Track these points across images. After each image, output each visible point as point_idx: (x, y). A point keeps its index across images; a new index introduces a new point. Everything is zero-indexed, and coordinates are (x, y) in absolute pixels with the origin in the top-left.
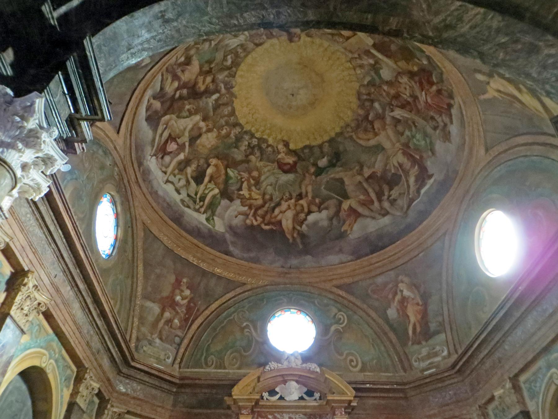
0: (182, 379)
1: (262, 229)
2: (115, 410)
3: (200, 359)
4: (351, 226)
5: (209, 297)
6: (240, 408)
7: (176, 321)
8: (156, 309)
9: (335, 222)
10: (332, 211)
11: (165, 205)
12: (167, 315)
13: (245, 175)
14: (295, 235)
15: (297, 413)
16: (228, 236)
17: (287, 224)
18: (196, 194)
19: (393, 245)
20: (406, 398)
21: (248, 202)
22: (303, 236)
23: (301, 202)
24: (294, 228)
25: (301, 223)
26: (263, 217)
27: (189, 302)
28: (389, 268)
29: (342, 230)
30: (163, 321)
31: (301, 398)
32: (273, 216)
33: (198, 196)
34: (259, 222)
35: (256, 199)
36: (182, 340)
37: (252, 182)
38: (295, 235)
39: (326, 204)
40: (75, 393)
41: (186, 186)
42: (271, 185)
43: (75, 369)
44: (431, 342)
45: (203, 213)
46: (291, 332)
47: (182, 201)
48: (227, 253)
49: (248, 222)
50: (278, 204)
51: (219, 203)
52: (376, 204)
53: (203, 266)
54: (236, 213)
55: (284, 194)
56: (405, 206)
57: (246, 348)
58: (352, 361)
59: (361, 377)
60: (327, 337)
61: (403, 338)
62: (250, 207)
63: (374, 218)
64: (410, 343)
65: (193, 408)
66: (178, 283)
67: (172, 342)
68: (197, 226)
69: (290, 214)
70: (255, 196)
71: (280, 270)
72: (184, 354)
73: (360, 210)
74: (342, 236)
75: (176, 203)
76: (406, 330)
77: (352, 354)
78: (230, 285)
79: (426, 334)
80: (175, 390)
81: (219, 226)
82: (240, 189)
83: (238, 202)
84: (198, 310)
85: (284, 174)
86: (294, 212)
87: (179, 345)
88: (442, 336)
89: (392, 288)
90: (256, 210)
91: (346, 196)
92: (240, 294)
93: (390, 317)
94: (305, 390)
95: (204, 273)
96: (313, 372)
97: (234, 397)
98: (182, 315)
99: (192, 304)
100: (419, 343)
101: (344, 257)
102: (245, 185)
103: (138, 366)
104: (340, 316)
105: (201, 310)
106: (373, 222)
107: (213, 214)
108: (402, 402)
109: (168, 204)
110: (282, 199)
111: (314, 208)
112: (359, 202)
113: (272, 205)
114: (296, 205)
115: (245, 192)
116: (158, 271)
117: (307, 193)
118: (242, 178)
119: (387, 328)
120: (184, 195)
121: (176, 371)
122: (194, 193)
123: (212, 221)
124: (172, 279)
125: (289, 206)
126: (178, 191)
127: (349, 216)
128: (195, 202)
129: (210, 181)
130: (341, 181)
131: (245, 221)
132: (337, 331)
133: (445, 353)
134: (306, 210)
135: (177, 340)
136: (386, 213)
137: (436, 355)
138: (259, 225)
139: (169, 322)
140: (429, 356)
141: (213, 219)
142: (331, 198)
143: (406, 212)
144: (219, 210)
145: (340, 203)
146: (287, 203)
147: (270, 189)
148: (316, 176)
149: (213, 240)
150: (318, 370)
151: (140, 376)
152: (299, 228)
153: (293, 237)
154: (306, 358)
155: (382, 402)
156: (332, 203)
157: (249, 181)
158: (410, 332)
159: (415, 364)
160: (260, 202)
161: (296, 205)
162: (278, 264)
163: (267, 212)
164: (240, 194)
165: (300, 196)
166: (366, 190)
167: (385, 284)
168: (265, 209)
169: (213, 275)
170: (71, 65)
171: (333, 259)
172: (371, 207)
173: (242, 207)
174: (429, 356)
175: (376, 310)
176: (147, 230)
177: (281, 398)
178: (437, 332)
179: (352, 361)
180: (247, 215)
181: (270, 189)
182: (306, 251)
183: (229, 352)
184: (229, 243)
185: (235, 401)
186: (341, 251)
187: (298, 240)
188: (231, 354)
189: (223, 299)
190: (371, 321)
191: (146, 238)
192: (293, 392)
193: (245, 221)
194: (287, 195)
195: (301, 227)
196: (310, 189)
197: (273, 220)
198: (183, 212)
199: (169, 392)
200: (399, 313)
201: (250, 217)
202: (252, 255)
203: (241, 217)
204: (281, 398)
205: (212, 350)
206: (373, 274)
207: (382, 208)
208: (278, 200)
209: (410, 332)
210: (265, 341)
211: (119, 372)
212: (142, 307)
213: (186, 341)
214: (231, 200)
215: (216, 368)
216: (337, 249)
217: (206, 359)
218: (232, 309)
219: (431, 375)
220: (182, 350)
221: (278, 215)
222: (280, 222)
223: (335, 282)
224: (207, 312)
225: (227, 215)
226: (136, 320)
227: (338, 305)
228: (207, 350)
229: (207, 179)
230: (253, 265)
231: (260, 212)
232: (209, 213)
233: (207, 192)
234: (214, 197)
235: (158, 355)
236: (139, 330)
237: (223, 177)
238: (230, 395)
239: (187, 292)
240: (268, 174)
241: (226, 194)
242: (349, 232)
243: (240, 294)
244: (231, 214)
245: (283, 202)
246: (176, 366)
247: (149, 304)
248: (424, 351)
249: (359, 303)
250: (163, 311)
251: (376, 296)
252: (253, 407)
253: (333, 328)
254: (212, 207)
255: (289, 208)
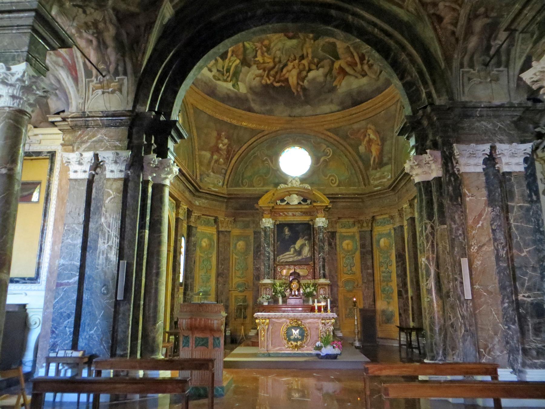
0: (228, 195)
1: (274, 87)
2: (196, 214)
3: (238, 182)
4: (340, 82)
5: (240, 142)
6: (263, 210)
7: (221, 160)
8: (208, 154)
9: (328, 78)
10: (327, 69)
11: (203, 84)
12: (215, 157)
13: (259, 45)
14: (299, 89)
15: (297, 211)
16: (250, 96)
17: (293, 80)
18: (223, 68)
19: (366, 103)
20: (363, 202)
21: (263, 66)
22: (304, 89)
23: (303, 62)
24: (298, 84)
25: (303, 79)
26: (274, 77)
27: (228, 147)
28: (363, 119)
29: (334, 85)
30: (213, 161)
31: (300, 203)
32: (282, 74)
33: (225, 69)
34: (271, 81)
35: (268, 63)
36: (226, 171)
37: (264, 49)
38: (299, 89)
39: (322, 64)
40: (177, 213)
41: (215, 64)
42: (279, 50)
43: (174, 202)
44: (383, 169)
45: (230, 82)
46: (295, 162)
47: (214, 76)
48: (250, 110)
49: (263, 82)
50: (285, 65)
51: (241, 71)
52: (359, 66)
53: (234, 122)
54: (254, 76)
55: (290, 56)
56: (378, 71)
57: (268, 173)
58: (332, 180)
59: (337, 190)
60: (318, 165)
61: (367, 166)
62: (264, 70)
63: (356, 77)
64: (371, 169)
65: (237, 209)
66: (219, 137)
67: (220, 173)
68: (227, 93)
69: (295, 72)
70: (267, 60)
71: (288, 118)
72: (228, 180)
73: (348, 69)
74: (333, 90)
75: (210, 81)
76: (370, 160)
77: (333, 176)
78: (253, 132)
79: (381, 164)
80: (226, 200)
81: (242, 89)
82: (256, 56)
83: (254, 67)
84: (234, 151)
85: (289, 40)
86: (298, 71)
87: (225, 174)
88: (390, 166)
89: (363, 132)
90: (269, 71)
91: (337, 58)
92: (260, 138)
93: (360, 151)
94: (302, 198)
95: (236, 127)
96: (307, 189)
97: (260, 205)
98: (225, 156)
99: (230, 148)
100: (376, 169)
101: (334, 107)
102: (259, 53)
103: (204, 191)
104: (328, 151)
105: (236, 150)
106: (356, 80)
107: (237, 80)
108: (360, 204)
109: (205, 83)
110: (288, 60)
111: (314, 67)
112: (347, 62)
113: (281, 66)
114: (299, 65)
115: (259, 58)
116: (205, 131)
117: (307, 54)
118: (256, 48)
119: (357, 158)
120: (214, 70)
121: (224, 191)
122: (222, 66)
123: (237, 86)
124: (215, 134)
125: (294, 66)
126: (210, 70)
127: (339, 73)
128: (223, 74)
129: (232, 55)
130: (334, 45)
131: (261, 82)
132: (325, 161)
133: (390, 177)
134: (307, 68)
135: (223, 171)
136: (364, 75)
137: (384, 177)
138: (272, 84)
139: (217, 161)
140: (380, 178)
141: (237, 84)
142: (325, 58)
143: (378, 76)
144: (241, 76)
145: (333, 63)
146: (292, 64)
147: (278, 53)
148: (315, 41)
149: (239, 102)
150: (310, 188)
151: (204, 195)
152: (301, 83)
153: (297, 91)
154: (303, 180)
155: (349, 204)
156: (326, 62)
157: (261, 49)
158: (372, 162)
159: (372, 182)
160: (271, 65)
161: (299, 65)
162: (286, 114)
163: (277, 73)
164: (256, 61)
165: (302, 58)
166: (352, 54)
167: (359, 130)
168: (275, 70)
169: (241, 127)
170: (173, 133)
171: (326, 108)
172: (355, 68)
173: (258, 71)
174: (380, 178)
175: (351, 145)
176: (195, 109)
177: (288, 203)
178: (386, 164)
179: (332, 180)
180: (261, 76)
181: (278, 53)
182: (307, 102)
183: (256, 177)
184: (251, 100)
185: (261, 207)
186: (332, 102)
187: (301, 94)
188: (257, 178)
189: (250, 142)
190: (348, 154)
191: (195, 112)
192: (295, 200)
193: (261, 82)
194: (292, 57)
195: (303, 82)
196: (310, 51)
197: (282, 78)
198: (216, 85)
199: (223, 202)
200: (366, 149)
201: (265, 77)
202: (268, 108)
203: (258, 79)
204: (288, 203)
205: (245, 176)
206: (352, 122)
207: (363, 70)
208: (285, 61)
209: (372, 162)
210: (278, 169)
211: (194, 195)
212: (199, 155)
213: (229, 171)
214: (249, 66)
215: (248, 187)
216: (329, 100)
217: (242, 182)
218: (256, 149)
219: (377, 191)
220: (227, 177)
221: (286, 73)
222: (287, 80)
223: (326, 127)
224: (240, 152)
225: (247, 79)
226: (197, 164)
227: (327, 143)
228: (243, 176)
229: (229, 54)
230: (267, 117)
231: (272, 73)
232: (234, 79)
233: (231, 64)
234: (236, 66)
235: (214, 182)
236: (200, 170)
237: (242, 49)
238: (258, 204)
239: (226, 141)
240: (276, 41)
241: (245, 62)
242: (338, 87)
243: (260, 138)
244: (251, 77)
245: (289, 63)
246: (225, 187)
247: (203, 153)
248: (378, 175)
249: (341, 141)
250: (212, 155)
251: (352, 137)
252: (271, 210)
253: (322, 159)
254: (236, 74)
255: (294, 67)
